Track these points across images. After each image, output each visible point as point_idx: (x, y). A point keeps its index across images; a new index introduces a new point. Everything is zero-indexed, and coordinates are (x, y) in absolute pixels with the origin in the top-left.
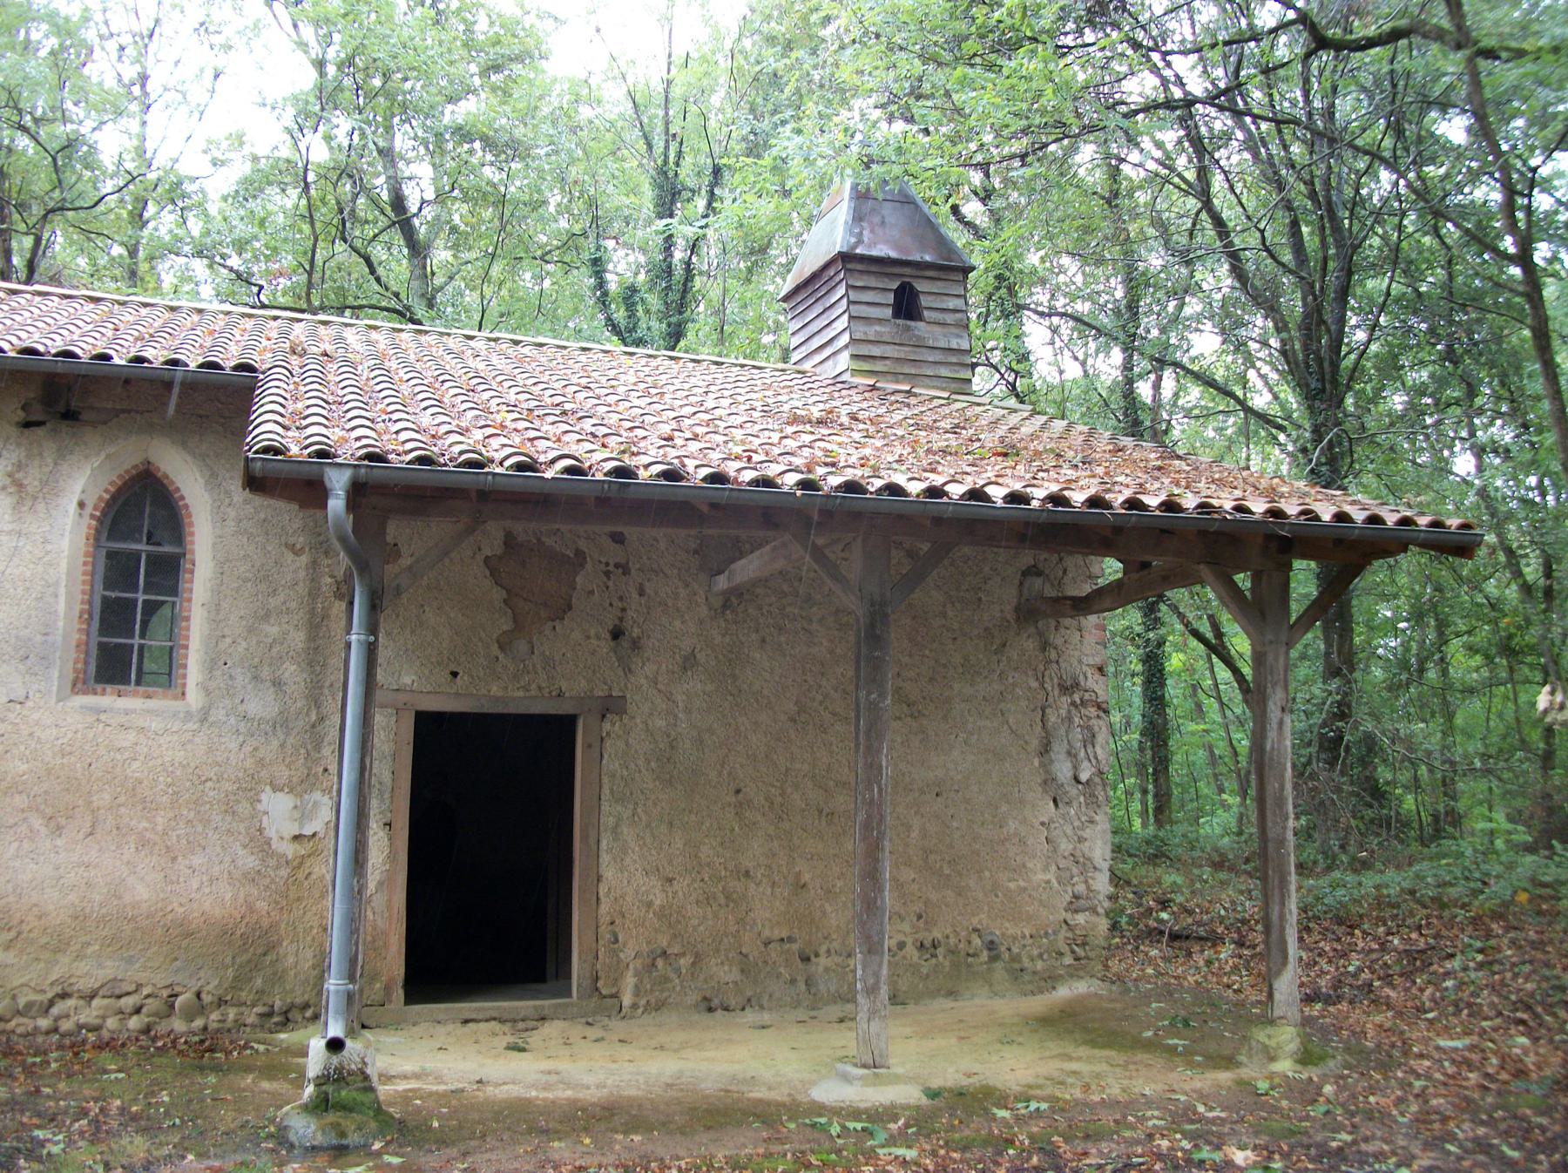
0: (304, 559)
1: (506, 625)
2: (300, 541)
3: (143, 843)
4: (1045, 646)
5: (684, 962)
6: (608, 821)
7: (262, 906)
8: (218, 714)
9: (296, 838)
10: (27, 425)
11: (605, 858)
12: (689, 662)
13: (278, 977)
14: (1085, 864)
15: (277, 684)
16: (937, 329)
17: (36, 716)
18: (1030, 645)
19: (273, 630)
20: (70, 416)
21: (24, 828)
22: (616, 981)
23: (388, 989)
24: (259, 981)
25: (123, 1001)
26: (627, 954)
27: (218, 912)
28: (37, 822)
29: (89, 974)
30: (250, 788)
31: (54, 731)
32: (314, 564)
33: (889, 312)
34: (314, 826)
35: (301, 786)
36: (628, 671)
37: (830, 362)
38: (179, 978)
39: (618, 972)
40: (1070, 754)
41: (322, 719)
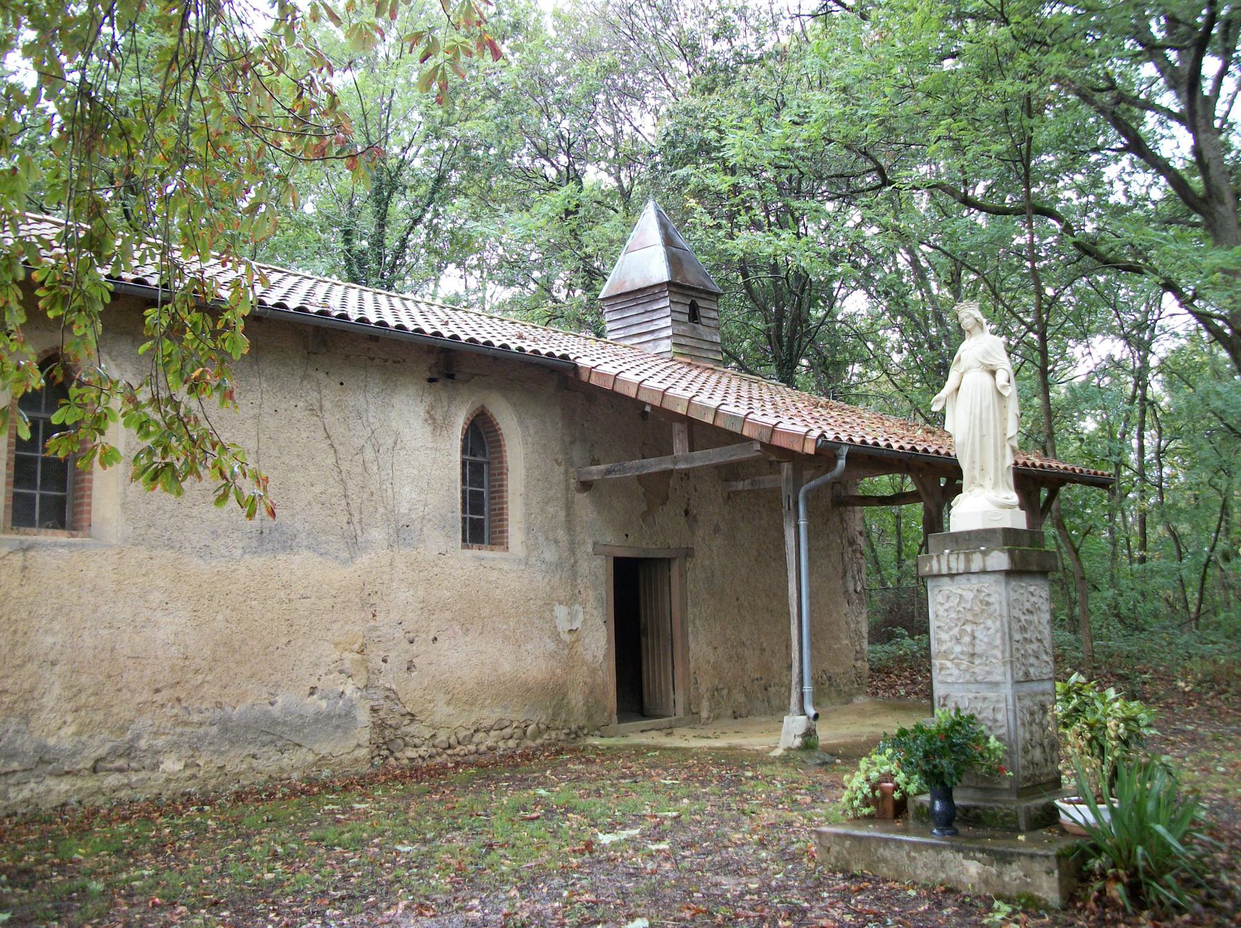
0: (562, 469)
1: (644, 507)
2: (560, 457)
3: (506, 638)
4: (842, 520)
5: (725, 692)
6: (691, 617)
7: (558, 671)
8: (532, 560)
9: (570, 631)
10: (431, 380)
11: (691, 637)
12: (717, 529)
13: (570, 712)
14: (858, 633)
15: (556, 542)
16: (707, 329)
17: (451, 562)
18: (837, 519)
19: (551, 510)
20: (451, 377)
21: (450, 632)
22: (698, 705)
23: (610, 716)
24: (563, 715)
25: (505, 731)
26: (702, 689)
27: (540, 677)
28: (457, 628)
29: (489, 716)
30: (548, 605)
31: (460, 571)
32: (566, 472)
33: (686, 318)
34: (576, 625)
35: (570, 601)
36: (693, 534)
37: (651, 344)
38: (528, 716)
39: (699, 698)
40: (854, 578)
41: (576, 562)
